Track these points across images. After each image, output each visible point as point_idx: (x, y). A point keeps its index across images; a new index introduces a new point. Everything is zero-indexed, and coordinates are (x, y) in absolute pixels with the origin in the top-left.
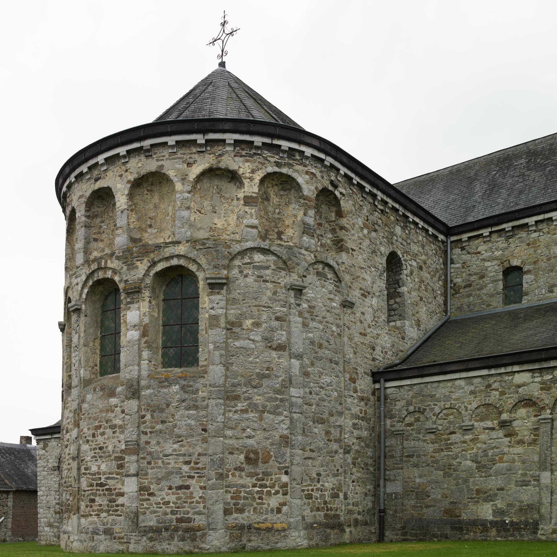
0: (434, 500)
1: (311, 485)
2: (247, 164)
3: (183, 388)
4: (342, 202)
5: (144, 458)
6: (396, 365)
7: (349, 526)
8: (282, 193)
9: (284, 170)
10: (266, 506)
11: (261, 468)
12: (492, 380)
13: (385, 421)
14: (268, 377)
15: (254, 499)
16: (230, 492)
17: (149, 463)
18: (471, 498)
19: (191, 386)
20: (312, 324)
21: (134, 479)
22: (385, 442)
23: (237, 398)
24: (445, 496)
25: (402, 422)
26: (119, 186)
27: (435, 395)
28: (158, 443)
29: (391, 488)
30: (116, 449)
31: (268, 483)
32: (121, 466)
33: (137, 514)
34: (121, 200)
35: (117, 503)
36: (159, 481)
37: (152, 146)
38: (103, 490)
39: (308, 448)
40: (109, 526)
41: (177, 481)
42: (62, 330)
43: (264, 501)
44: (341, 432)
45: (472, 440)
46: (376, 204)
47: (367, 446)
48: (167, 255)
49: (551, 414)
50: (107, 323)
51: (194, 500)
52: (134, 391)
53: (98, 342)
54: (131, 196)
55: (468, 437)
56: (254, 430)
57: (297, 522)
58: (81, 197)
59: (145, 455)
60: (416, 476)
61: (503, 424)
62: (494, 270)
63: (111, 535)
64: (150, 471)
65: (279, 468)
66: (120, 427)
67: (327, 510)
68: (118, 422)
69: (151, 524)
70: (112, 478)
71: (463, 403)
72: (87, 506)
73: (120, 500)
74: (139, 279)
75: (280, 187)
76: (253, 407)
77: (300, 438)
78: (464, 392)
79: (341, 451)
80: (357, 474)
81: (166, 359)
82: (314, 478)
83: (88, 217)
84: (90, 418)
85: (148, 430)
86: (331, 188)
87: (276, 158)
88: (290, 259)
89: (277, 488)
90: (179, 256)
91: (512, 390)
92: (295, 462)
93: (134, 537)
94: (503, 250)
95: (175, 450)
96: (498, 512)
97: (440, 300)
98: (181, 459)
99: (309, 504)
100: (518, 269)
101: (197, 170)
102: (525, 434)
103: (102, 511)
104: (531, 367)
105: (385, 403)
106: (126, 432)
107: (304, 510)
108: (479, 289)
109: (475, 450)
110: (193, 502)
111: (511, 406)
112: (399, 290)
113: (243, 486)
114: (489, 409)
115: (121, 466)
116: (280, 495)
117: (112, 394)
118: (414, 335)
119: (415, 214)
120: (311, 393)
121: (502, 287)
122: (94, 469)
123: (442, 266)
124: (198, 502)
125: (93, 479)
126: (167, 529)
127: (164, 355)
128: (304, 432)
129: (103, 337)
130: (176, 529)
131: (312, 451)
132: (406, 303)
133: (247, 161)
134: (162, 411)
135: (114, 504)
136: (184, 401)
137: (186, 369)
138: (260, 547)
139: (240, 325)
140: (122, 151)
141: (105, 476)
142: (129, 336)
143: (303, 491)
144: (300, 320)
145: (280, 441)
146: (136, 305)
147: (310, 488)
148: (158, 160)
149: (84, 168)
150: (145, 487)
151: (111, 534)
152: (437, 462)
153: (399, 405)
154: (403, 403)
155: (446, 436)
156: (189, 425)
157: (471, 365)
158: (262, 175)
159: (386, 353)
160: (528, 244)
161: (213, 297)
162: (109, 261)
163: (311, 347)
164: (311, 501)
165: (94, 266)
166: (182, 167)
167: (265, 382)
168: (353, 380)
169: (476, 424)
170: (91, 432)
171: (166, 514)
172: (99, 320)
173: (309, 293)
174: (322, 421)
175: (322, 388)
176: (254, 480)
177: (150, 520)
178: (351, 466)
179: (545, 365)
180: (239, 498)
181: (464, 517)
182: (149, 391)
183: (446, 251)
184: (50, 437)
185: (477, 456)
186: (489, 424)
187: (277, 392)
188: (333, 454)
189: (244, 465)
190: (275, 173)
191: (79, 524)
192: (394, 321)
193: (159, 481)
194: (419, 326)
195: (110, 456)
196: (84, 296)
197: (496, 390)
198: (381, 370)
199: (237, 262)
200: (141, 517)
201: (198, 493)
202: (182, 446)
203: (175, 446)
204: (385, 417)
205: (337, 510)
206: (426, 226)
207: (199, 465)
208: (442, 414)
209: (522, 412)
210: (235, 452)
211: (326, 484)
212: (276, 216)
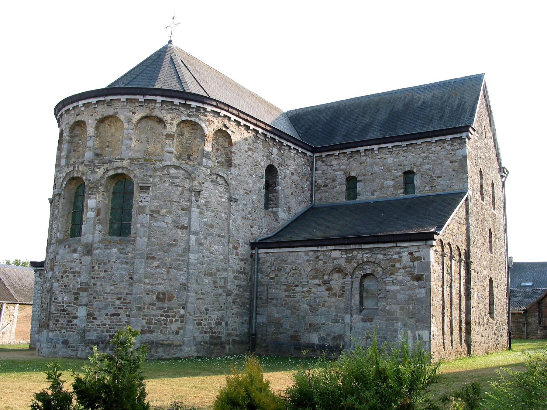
0: (286, 329)
1: (201, 317)
2: (169, 115)
3: (119, 250)
4: (232, 137)
5: (91, 294)
6: (268, 238)
7: (229, 344)
8: (192, 131)
9: (193, 119)
10: (169, 329)
11: (166, 305)
12: (319, 254)
13: (257, 275)
14: (175, 245)
15: (161, 324)
16: (145, 319)
17: (95, 298)
18: (307, 329)
19: (124, 249)
20: (206, 213)
21: (84, 308)
22: (257, 289)
23: (153, 258)
24: (291, 327)
25: (268, 276)
26: (90, 121)
27: (287, 260)
28: (102, 285)
29: (261, 319)
31: (171, 314)
32: (77, 299)
33: (84, 331)
34: (91, 130)
35: (73, 323)
36: (100, 310)
37: (111, 100)
39: (200, 292)
40: (66, 338)
41: (112, 311)
42: (51, 203)
43: (168, 326)
44: (225, 282)
45: (308, 291)
46: (258, 136)
47: (245, 291)
49: (351, 278)
50: (77, 204)
51: (122, 324)
52: (89, 250)
53: (70, 215)
54: (97, 128)
55: (305, 289)
56: (164, 279)
57: (190, 340)
58: (67, 124)
59: (92, 292)
60: (274, 312)
61: (325, 282)
62: (341, 177)
64: (95, 303)
65: (179, 305)
66: (79, 273)
67: (212, 333)
68: (78, 269)
69: (93, 338)
70: (71, 306)
71: (303, 267)
72: (54, 324)
73: (75, 321)
74: (97, 180)
75: (191, 127)
76: (163, 265)
77: (194, 286)
78: (303, 260)
79: (225, 294)
80: (236, 309)
81: (112, 231)
82: (204, 312)
83: (71, 136)
84: (60, 265)
86: (224, 129)
87: (188, 112)
88: (193, 173)
89: (176, 318)
90: (123, 168)
91: (330, 261)
92: (189, 301)
95: (111, 290)
96: (321, 339)
97: (308, 194)
98: (115, 296)
99: (199, 329)
100: (354, 178)
101: (138, 116)
102: (337, 289)
103: (62, 328)
105: (258, 263)
106: (82, 276)
107: (195, 333)
108: (332, 189)
109: (309, 298)
110: (121, 325)
111: (329, 271)
112: (276, 188)
113: (154, 316)
114: (317, 274)
115: (77, 299)
116: (179, 323)
117: (75, 251)
118: (284, 217)
119: (287, 140)
120: (203, 257)
121: (345, 189)
122: (60, 299)
123: (310, 172)
125: (59, 306)
126: (102, 342)
127: (111, 228)
128: (197, 281)
129: (74, 213)
131: (202, 294)
132: (279, 197)
133: (170, 113)
134: (105, 264)
135: (71, 324)
137: (123, 238)
138: (163, 356)
139: (158, 212)
140: (93, 101)
142: (89, 215)
143: (195, 320)
144: (198, 210)
145: (181, 287)
146: (94, 196)
147: (200, 318)
148: (114, 109)
149: (70, 107)
150: (91, 313)
151: (67, 344)
153: (267, 265)
154: (268, 264)
155: (293, 288)
156: (122, 275)
157: (307, 244)
158: (178, 122)
159: (262, 229)
160: (361, 163)
161: (142, 195)
162: (80, 167)
163: (205, 227)
164: (200, 327)
165: (71, 168)
166: (130, 114)
167: (173, 249)
168: (235, 248)
169: (310, 281)
170: (60, 275)
172: (73, 201)
173: (205, 194)
174: (211, 274)
175: (212, 253)
176: (162, 312)
177: (92, 336)
178: (232, 304)
179: (348, 247)
180: (151, 323)
181: (302, 341)
183: (313, 162)
185: (310, 302)
186: (317, 281)
187: (180, 255)
188: (219, 296)
189: (156, 302)
190: (187, 120)
191: (48, 336)
192: (272, 208)
194: (290, 211)
196: (64, 186)
197: (322, 260)
198: (257, 241)
199: (159, 173)
200: (87, 333)
201: (124, 319)
203: (112, 287)
204: (258, 272)
205: (220, 333)
206: (297, 148)
207: (127, 301)
208: (290, 273)
209: (336, 276)
210: (150, 293)
211: (212, 316)
212: (188, 145)
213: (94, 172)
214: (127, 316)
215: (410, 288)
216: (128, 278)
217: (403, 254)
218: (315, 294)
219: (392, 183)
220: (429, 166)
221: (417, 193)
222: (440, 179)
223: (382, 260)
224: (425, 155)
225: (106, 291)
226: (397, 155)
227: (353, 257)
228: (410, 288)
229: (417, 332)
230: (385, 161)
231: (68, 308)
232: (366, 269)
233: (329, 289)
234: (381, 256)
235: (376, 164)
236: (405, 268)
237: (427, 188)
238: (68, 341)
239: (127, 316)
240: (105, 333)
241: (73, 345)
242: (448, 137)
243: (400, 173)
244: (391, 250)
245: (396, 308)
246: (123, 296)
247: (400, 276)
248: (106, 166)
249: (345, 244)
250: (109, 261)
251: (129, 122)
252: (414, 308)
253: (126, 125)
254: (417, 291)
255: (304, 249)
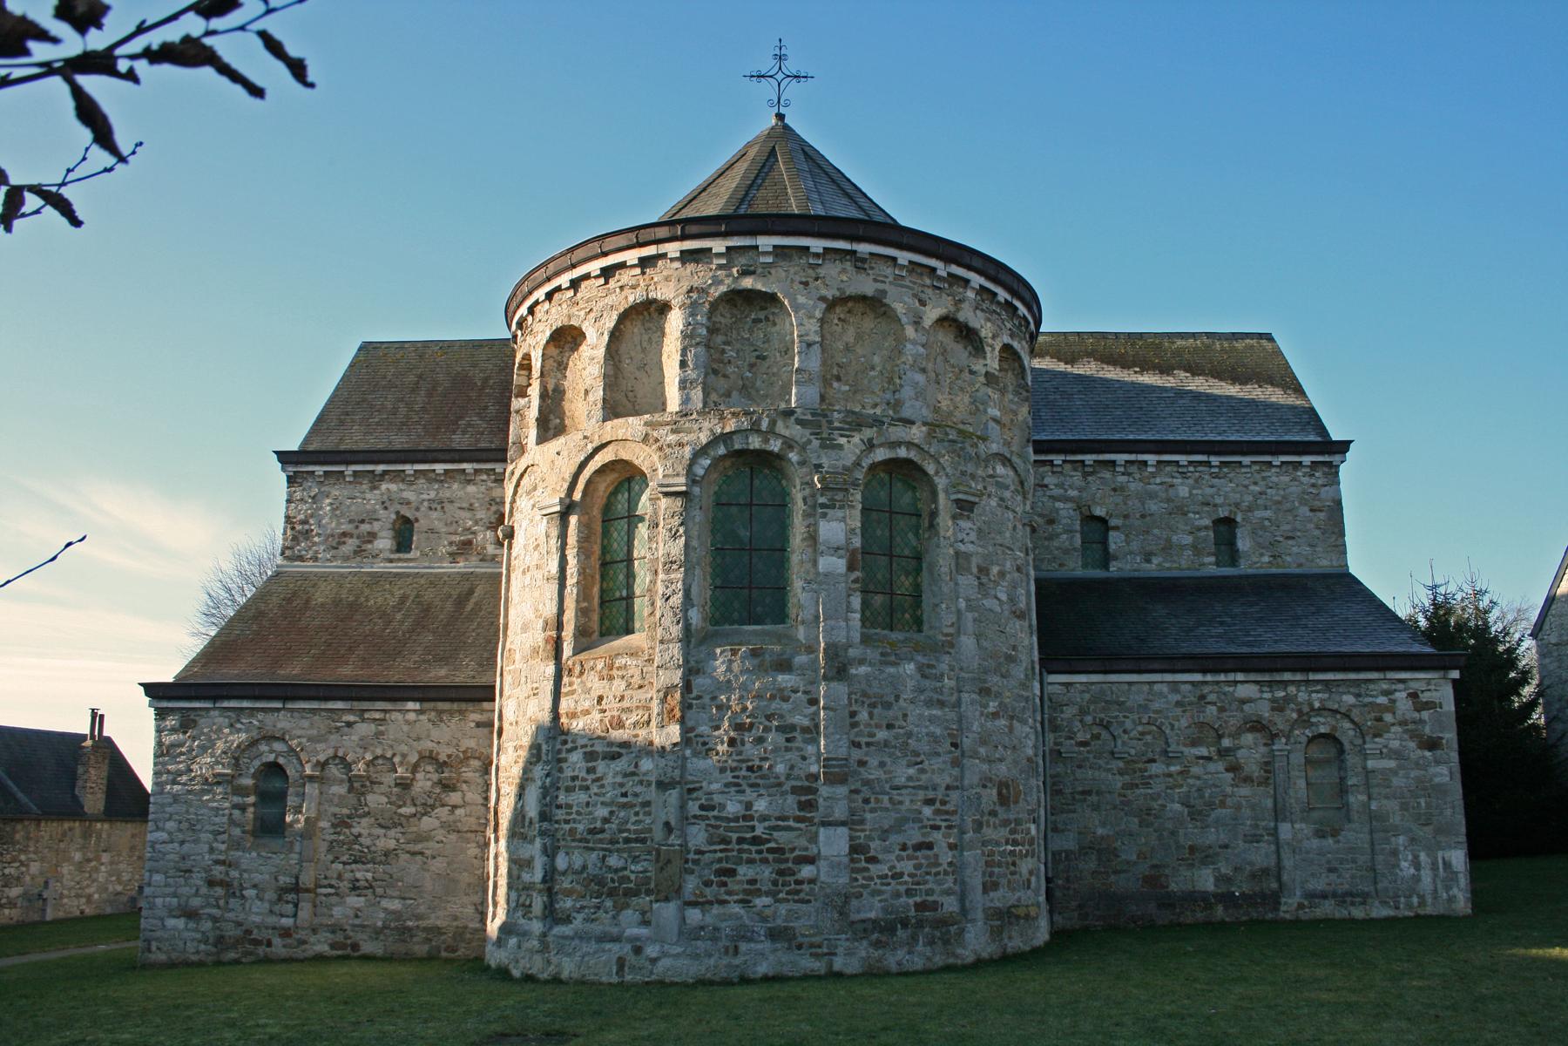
5: (856, 791)
12: (1206, 689)
17: (866, 801)
19: (932, 667)
28: (882, 764)
30: (796, 772)
35: (799, 876)
36: (885, 834)
38: (759, 852)
40: (779, 922)
41: (914, 835)
45: (1181, 773)
48: (893, 438)
51: (940, 869)
59: (858, 785)
61: (1223, 753)
63: (789, 941)
64: (868, 816)
66: (805, 730)
68: (800, 720)
69: (872, 915)
71: (1167, 718)
73: (806, 871)
81: (868, 614)
85: (863, 740)
90: (910, 445)
93: (843, 944)
94: (1080, 490)
95: (910, 778)
96: (1220, 879)
98: (921, 794)
102: (1253, 769)
104: (1259, 677)
109: (1184, 789)
114: (1204, 732)
115: (809, 806)
122: (733, 808)
124: (946, 873)
130: (920, 924)
134: (887, 706)
135: (791, 879)
136: (922, 691)
140: (817, 245)
141: (766, 824)
146: (840, 513)
152: (1128, 803)
153: (1069, 712)
160: (1114, 490)
171: (897, 895)
177: (871, 909)
179: (1277, 677)
181: (1173, 887)
182: (863, 670)
184: (208, 705)
186: (1203, 751)
193: (885, 834)
195: (780, 785)
197: (1214, 704)
201: (946, 857)
202: (923, 771)
203: (911, 771)
209: (1248, 738)
213: (828, 445)
214: (952, 847)
215: (1417, 764)
216: (947, 746)
217: (1397, 694)
218: (1198, 778)
219: (1188, 540)
220: (1268, 513)
221: (1244, 568)
222: (1290, 542)
223: (1354, 706)
224: (1257, 489)
225: (897, 782)
226: (1196, 481)
227: (1288, 699)
228: (1417, 764)
229: (1440, 854)
230: (1171, 491)
231: (775, 834)
232: (1316, 725)
233: (1233, 768)
234: (1349, 699)
235: (1152, 496)
236: (1403, 723)
237: (1266, 559)
238: (793, 928)
239: (952, 847)
240: (903, 899)
241: (817, 940)
242: (1307, 460)
243: (1207, 522)
244: (1371, 686)
245: (1392, 805)
246: (940, 795)
247: (1394, 739)
248: (868, 433)
249: (1270, 670)
250: (897, 698)
251: (917, 323)
252: (1428, 805)
253: (910, 331)
254: (1432, 770)
255: (1169, 677)
